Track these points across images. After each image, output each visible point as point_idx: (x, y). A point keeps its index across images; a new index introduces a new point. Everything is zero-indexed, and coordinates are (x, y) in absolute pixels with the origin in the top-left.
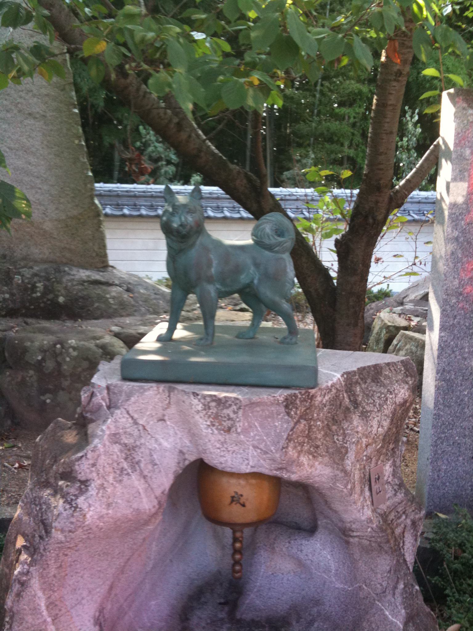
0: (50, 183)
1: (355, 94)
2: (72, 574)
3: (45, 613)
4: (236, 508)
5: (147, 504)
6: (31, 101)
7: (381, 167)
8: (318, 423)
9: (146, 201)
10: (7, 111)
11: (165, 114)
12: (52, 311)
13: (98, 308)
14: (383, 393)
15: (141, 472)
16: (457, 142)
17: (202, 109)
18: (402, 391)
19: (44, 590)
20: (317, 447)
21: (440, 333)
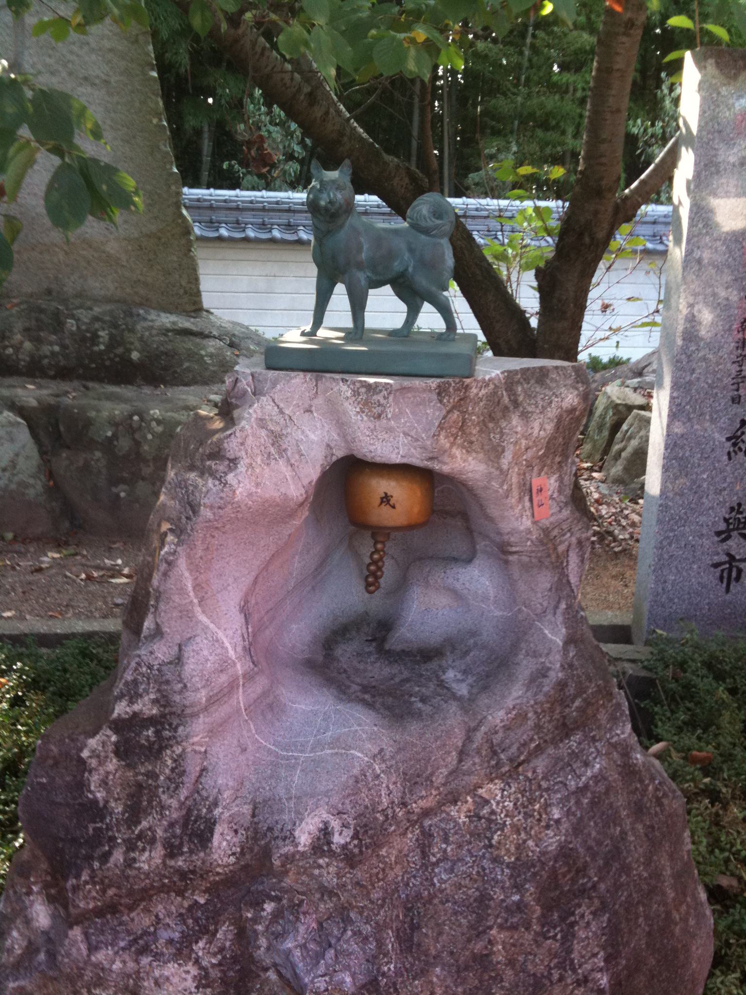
1: (586, 51)
3: (192, 594)
4: (385, 509)
5: (296, 491)
6: (87, 58)
7: (604, 160)
9: (254, 216)
10: (52, 74)
11: (292, 79)
12: (123, 372)
13: (188, 369)
15: (288, 460)
16: (703, 124)
17: (348, 74)
18: (570, 396)
19: (191, 571)
20: (472, 443)
21: (672, 393)
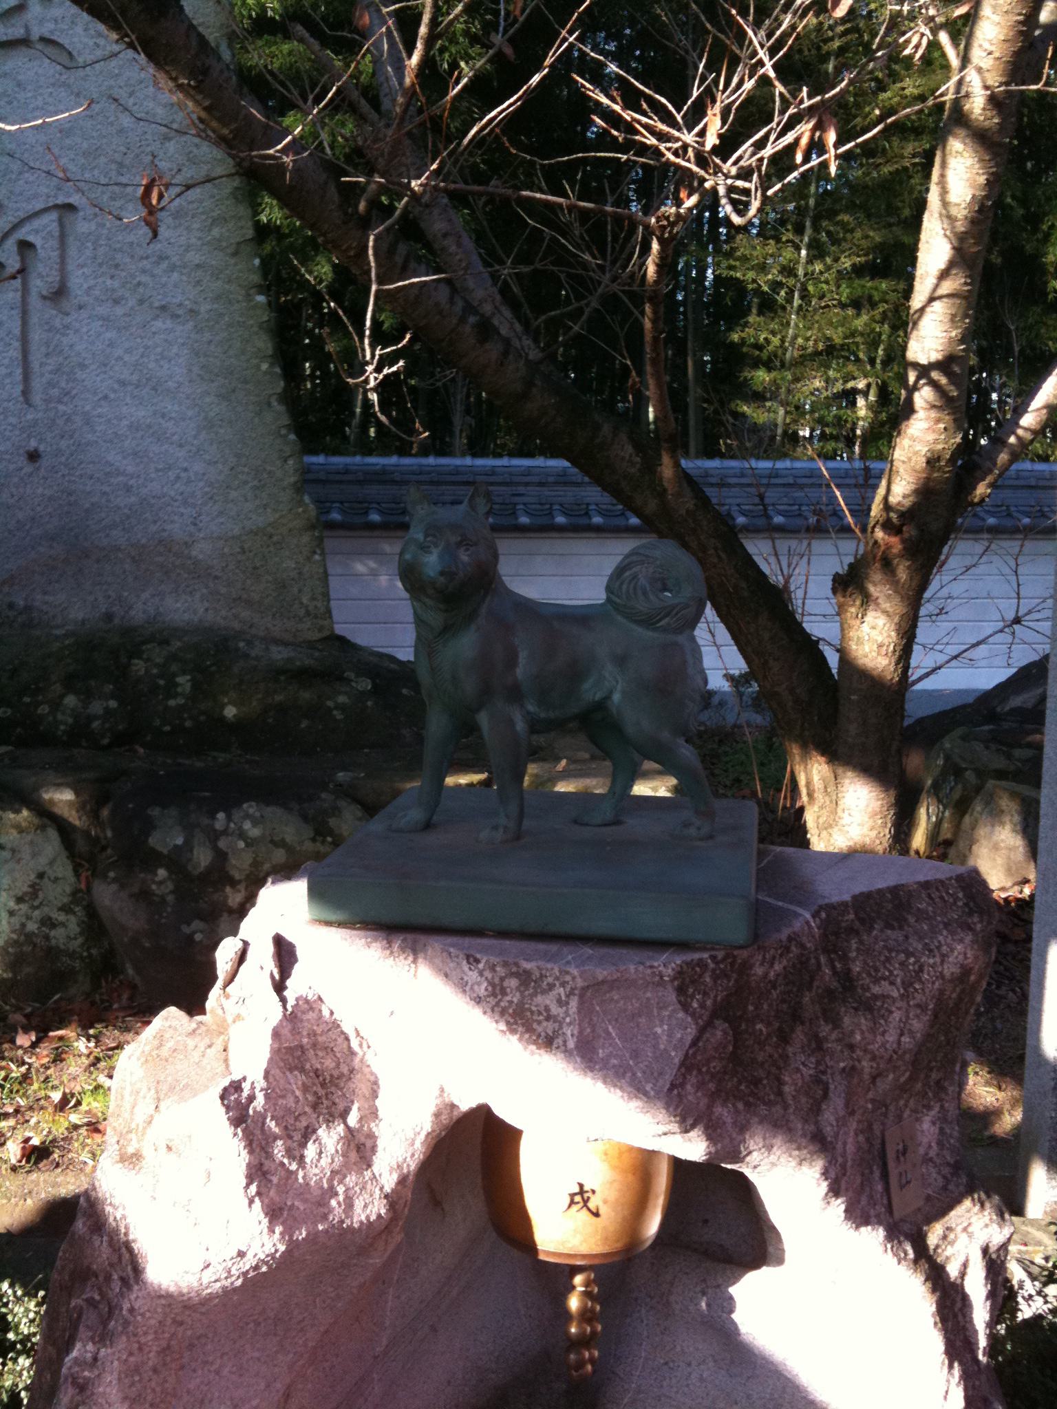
0: (207, 457)
2: (193, 1365)
8: (759, 1026)
14: (912, 954)
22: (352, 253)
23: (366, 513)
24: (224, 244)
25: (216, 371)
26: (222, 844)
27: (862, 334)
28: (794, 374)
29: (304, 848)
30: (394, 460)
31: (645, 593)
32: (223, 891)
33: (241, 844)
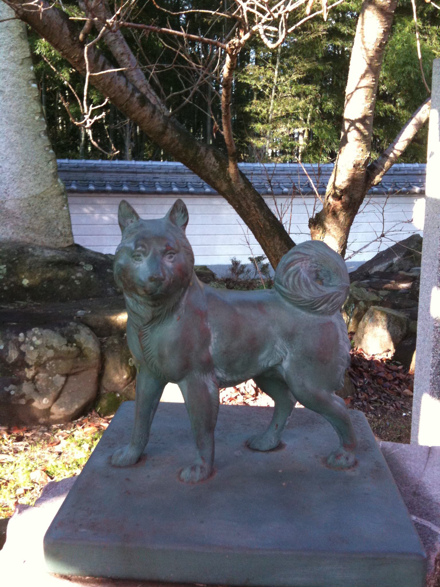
0: (11, 161)
22: (76, 60)
23: (88, 186)
24: (16, 59)
25: (14, 120)
26: (22, 348)
27: (301, 109)
28: (273, 126)
29: (62, 349)
30: (100, 161)
31: (307, 285)
32: (24, 370)
33: (32, 348)
